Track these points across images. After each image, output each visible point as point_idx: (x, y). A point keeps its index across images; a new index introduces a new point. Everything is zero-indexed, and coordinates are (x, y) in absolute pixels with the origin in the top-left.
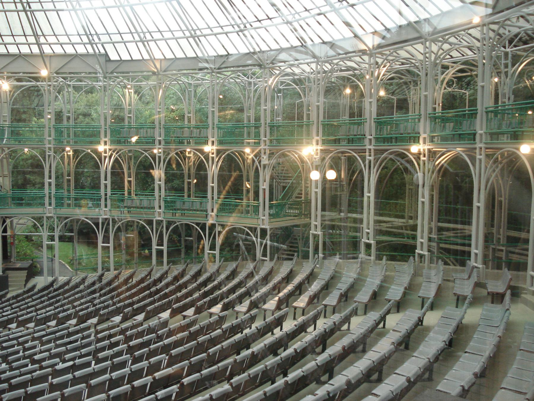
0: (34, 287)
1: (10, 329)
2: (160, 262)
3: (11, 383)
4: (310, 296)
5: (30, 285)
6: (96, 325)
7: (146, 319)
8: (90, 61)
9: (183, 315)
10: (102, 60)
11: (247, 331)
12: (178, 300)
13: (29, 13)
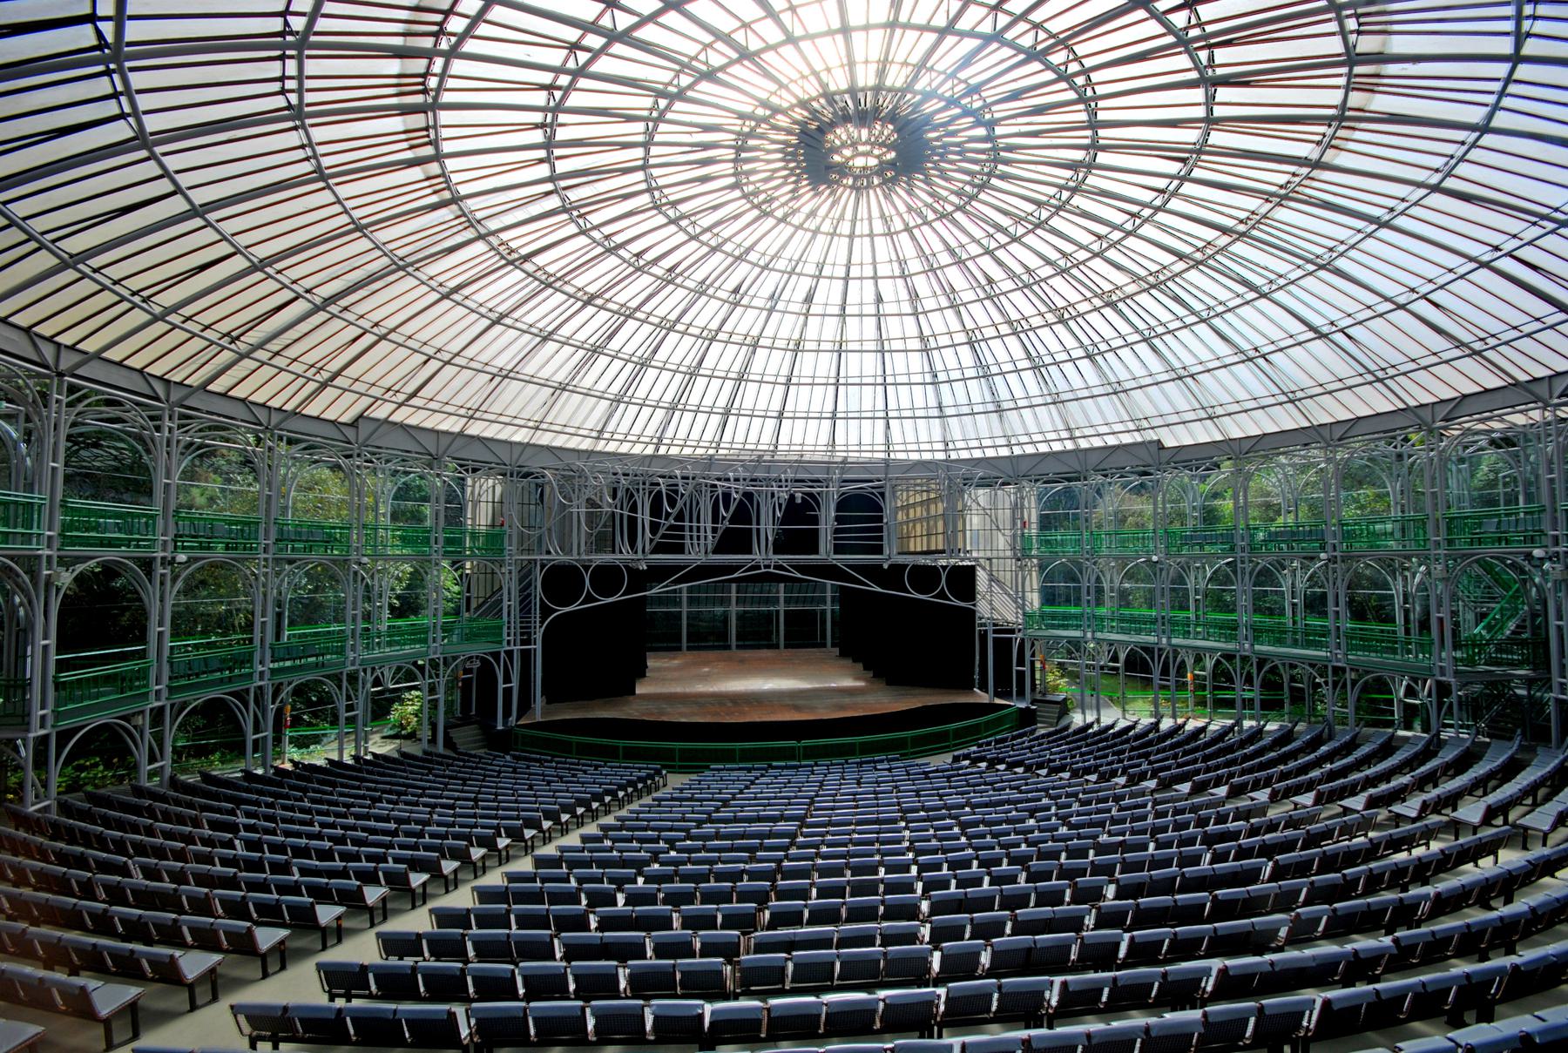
0: (1067, 728)
4: (904, 756)
5: (1063, 723)
6: (1153, 792)
10: (1154, 449)
11: (1418, 852)
12: (1284, 776)
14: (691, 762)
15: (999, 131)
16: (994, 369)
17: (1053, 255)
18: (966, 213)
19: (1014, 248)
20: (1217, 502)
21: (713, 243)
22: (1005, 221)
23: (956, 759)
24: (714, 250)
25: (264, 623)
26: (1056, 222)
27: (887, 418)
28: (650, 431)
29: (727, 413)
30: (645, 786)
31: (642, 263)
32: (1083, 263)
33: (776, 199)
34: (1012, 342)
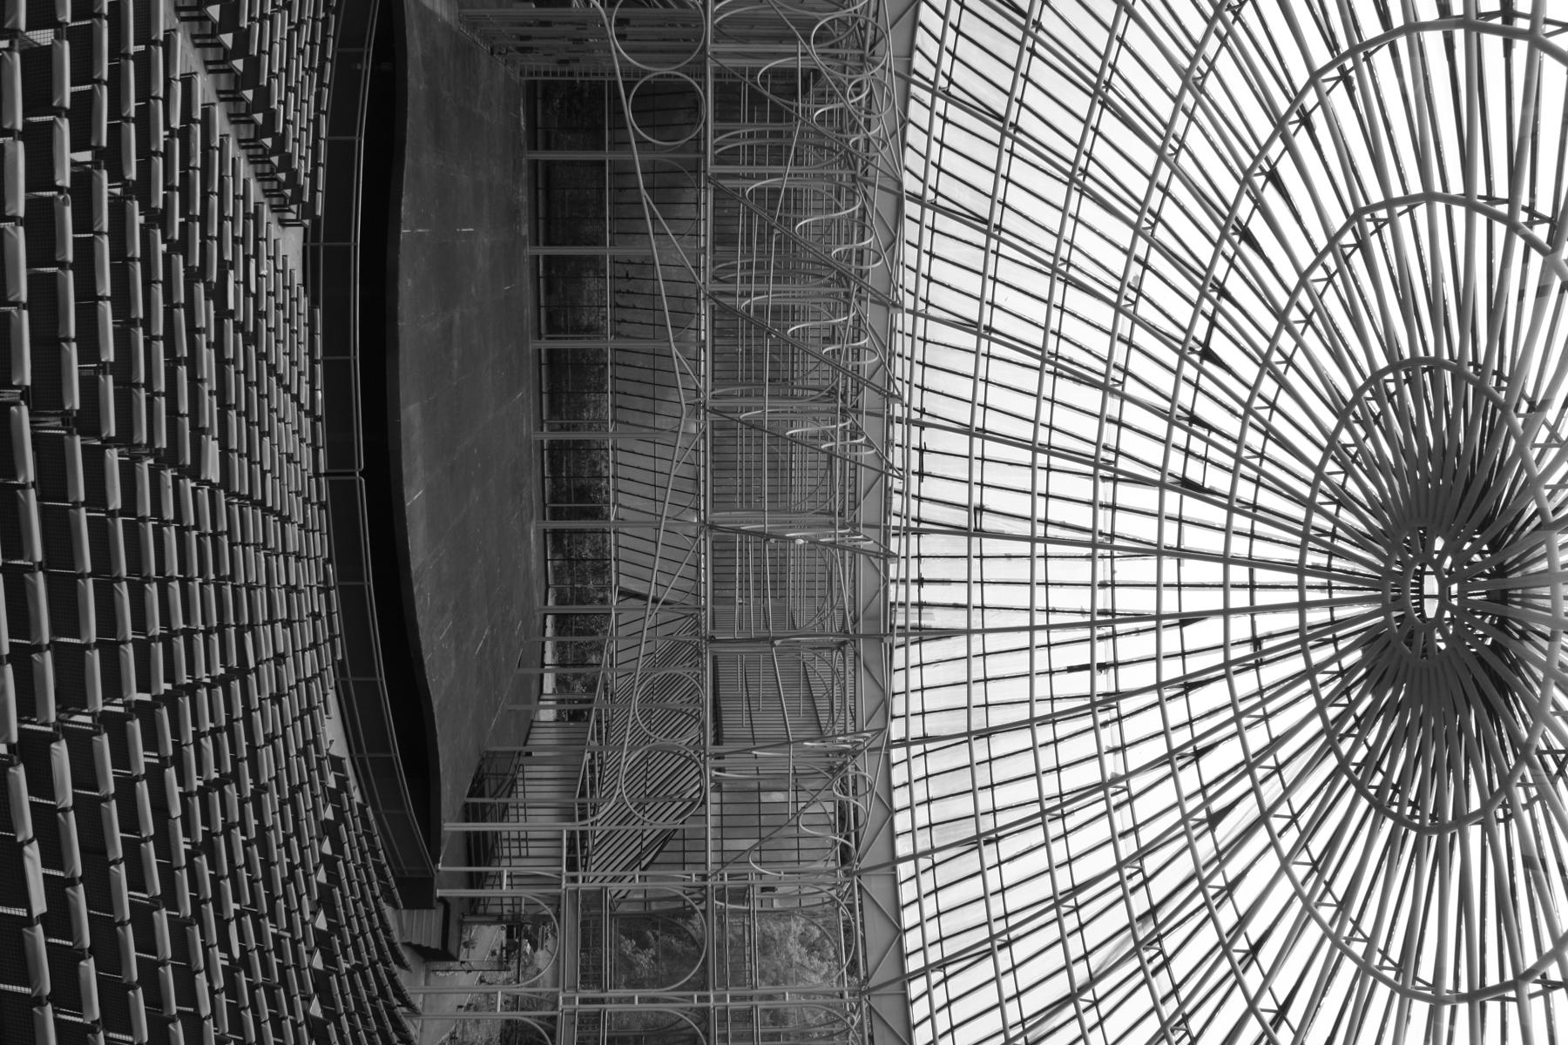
1: (314, 913)
3: (191, 925)
4: (340, 668)
5: (407, 956)
8: (883, 837)
13: (988, 946)
15: (1475, 832)
16: (1055, 828)
17: (1255, 930)
18: (1334, 776)
19: (1271, 862)
21: (1295, 315)
22: (1318, 845)
23: (337, 763)
24: (1281, 315)
26: (1313, 932)
27: (969, 632)
28: (947, 186)
29: (992, 229)
30: (268, 153)
31: (1259, 181)
32: (1239, 981)
33: (1370, 434)
34: (1105, 858)
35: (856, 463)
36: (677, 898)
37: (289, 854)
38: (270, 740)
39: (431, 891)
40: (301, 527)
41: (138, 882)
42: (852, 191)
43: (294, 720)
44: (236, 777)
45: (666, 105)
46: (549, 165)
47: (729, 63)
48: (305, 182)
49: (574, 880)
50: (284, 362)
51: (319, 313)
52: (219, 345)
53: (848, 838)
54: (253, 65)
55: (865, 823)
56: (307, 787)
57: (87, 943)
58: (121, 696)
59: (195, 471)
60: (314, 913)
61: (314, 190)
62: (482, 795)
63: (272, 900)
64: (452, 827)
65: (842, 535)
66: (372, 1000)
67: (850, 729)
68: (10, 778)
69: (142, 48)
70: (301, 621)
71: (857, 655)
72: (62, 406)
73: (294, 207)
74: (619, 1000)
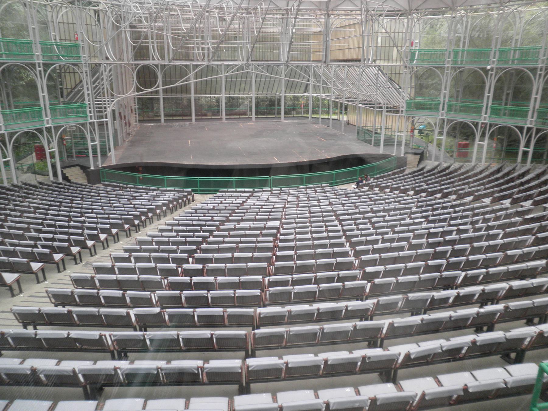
2: (524, 160)
4: (332, 184)
5: (421, 166)
7: (473, 201)
9: (544, 207)
14: (207, 188)
20: (464, 142)
25: (489, 93)
35: (267, 9)
36: (411, 77)
37: (391, 202)
38: (357, 207)
39: (401, 158)
40: (288, 195)
41: (401, 249)
42: (171, 10)
43: (349, 200)
44: (369, 218)
45: (146, 77)
46: (165, 115)
47: (130, 55)
48: (181, 194)
49: (402, 111)
50: (238, 201)
51: (221, 190)
52: (239, 221)
53: (398, 14)
54: (150, 210)
55: (393, 8)
56: (370, 196)
57: (423, 263)
58: (348, 252)
59: (278, 229)
60: (408, 195)
61: (183, 191)
62: (371, 140)
63: (405, 208)
64: (381, 150)
65: (291, 14)
66: (436, 178)
67: (359, 12)
68: (412, 299)
69: (154, 243)
70: (318, 197)
71: (332, 10)
72: (266, 267)
73: (189, 197)
74: (445, 97)
